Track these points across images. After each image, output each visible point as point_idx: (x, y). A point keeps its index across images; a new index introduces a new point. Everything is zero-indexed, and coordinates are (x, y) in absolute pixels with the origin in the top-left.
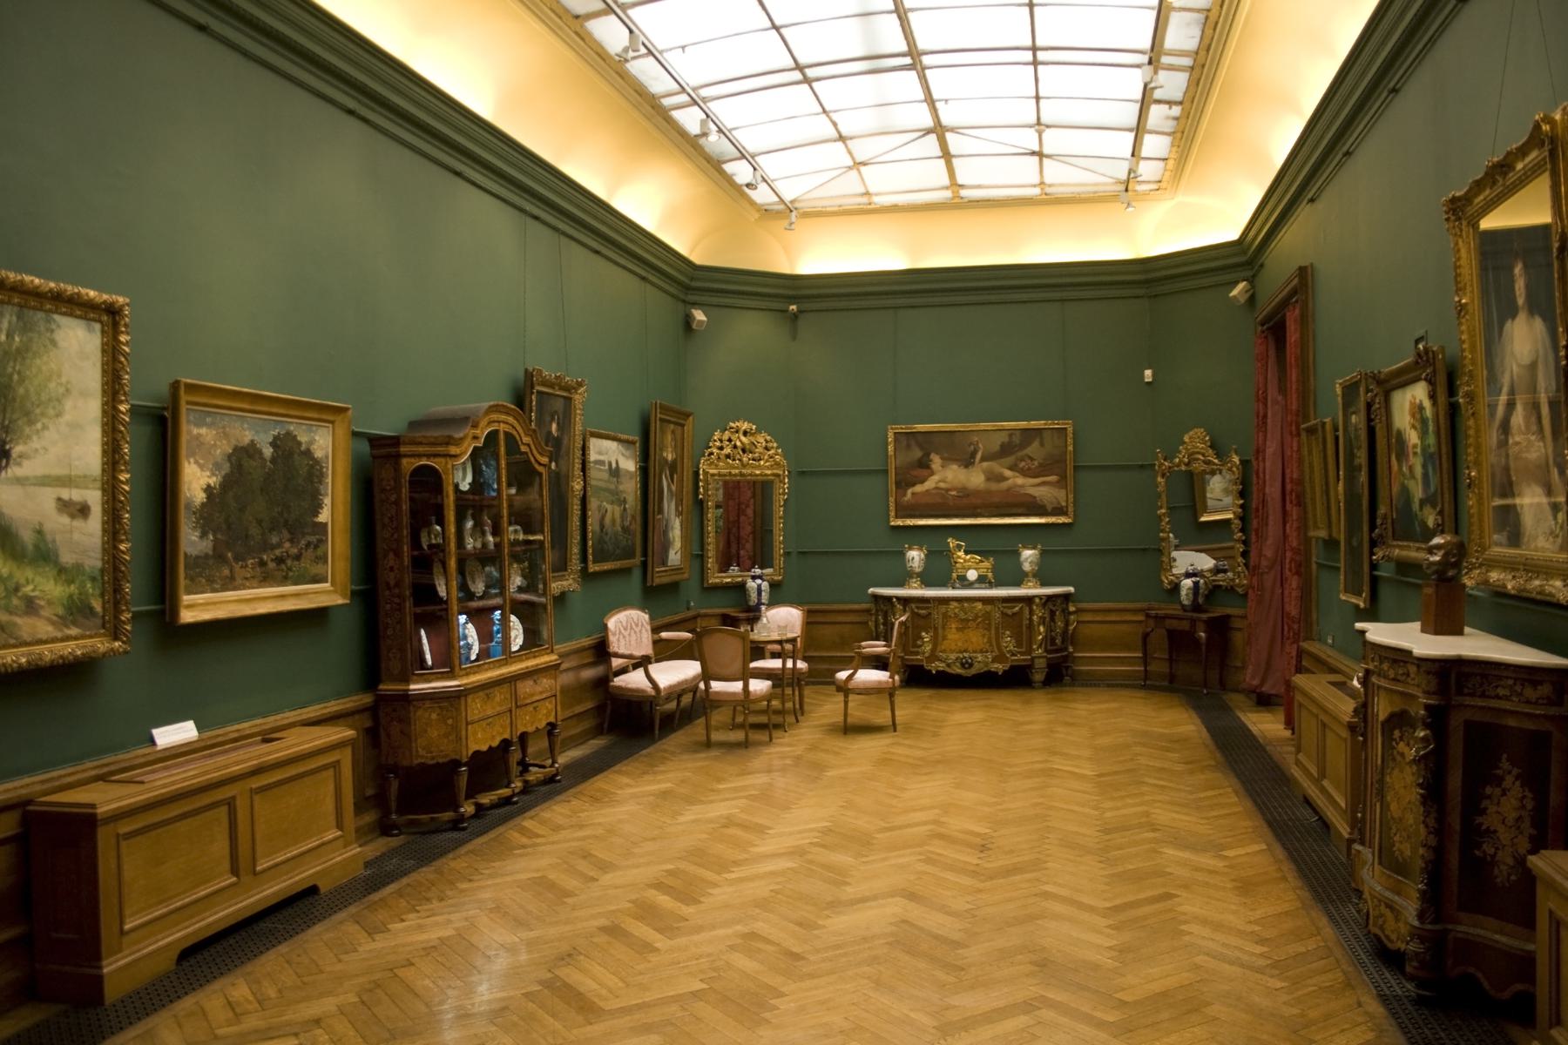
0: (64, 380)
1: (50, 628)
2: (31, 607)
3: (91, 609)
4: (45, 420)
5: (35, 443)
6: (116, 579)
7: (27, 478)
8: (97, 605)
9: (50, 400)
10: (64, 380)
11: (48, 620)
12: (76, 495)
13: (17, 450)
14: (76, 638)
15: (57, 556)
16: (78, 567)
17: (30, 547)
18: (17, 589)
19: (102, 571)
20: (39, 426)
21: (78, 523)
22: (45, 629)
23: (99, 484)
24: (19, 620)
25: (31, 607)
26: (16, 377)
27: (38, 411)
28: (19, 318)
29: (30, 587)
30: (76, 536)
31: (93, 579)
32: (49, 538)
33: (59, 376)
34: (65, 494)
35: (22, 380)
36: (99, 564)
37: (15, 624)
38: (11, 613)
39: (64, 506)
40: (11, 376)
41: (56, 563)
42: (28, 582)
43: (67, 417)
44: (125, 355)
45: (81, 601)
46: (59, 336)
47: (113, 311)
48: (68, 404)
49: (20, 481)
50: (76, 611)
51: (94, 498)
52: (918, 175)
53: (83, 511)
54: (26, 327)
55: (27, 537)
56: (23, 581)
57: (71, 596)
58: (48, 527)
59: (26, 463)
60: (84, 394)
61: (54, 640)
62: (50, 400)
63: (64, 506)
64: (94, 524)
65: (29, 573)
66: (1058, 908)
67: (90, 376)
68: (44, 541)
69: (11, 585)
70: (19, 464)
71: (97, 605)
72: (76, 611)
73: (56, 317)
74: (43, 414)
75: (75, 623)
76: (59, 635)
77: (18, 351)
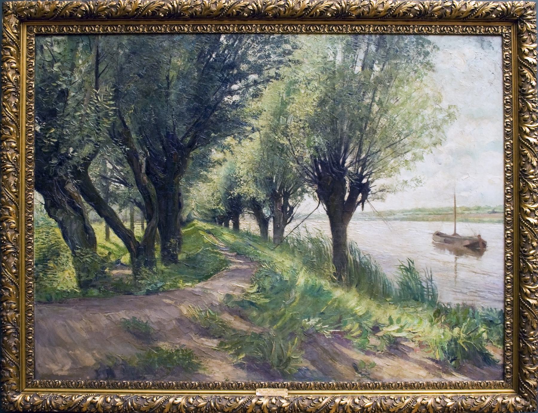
0: (444, 105)
1: (423, 373)
2: (395, 348)
3: (487, 358)
4: (417, 151)
5: (404, 174)
6: (520, 326)
7: (391, 213)
8: (496, 354)
9: (425, 127)
10: (444, 105)
11: (421, 364)
12: (465, 230)
13: (376, 185)
14: (455, 386)
15: (434, 296)
16: (467, 311)
17: (396, 286)
18: (376, 329)
19: (504, 314)
20: (409, 156)
21: (468, 261)
22: (412, 372)
23: (501, 217)
24: (378, 362)
25: (395, 348)
26: (375, 108)
27: (406, 141)
28: (378, 46)
29: (396, 327)
30: (462, 275)
31: (490, 323)
32: (423, 276)
33: (439, 101)
34: (447, 229)
35: (384, 111)
36: (500, 307)
37: (373, 365)
38: (368, 353)
39: (444, 241)
40: (369, 107)
41: (433, 302)
42: (391, 323)
43: (449, 145)
44: (531, 66)
45: (469, 346)
46: (436, 58)
47: (512, 19)
48: (452, 130)
49: (383, 216)
50: (463, 357)
51: (494, 234)
52: (102, 41)
53: (477, 247)
54: (389, 56)
55: (392, 276)
56: (384, 320)
57: (454, 340)
58: (420, 264)
59: (389, 197)
60: (478, 118)
61: (429, 386)
62: (425, 127)
63: (444, 241)
64: (493, 264)
65: (394, 312)
66: (496, 292)
67: (491, 98)
68: (418, 281)
69: (369, 324)
70: (382, 199)
71: (496, 354)
72: (463, 357)
73: (431, 38)
74: (414, 144)
75: (459, 370)
76: (436, 380)
77: (379, 81)
